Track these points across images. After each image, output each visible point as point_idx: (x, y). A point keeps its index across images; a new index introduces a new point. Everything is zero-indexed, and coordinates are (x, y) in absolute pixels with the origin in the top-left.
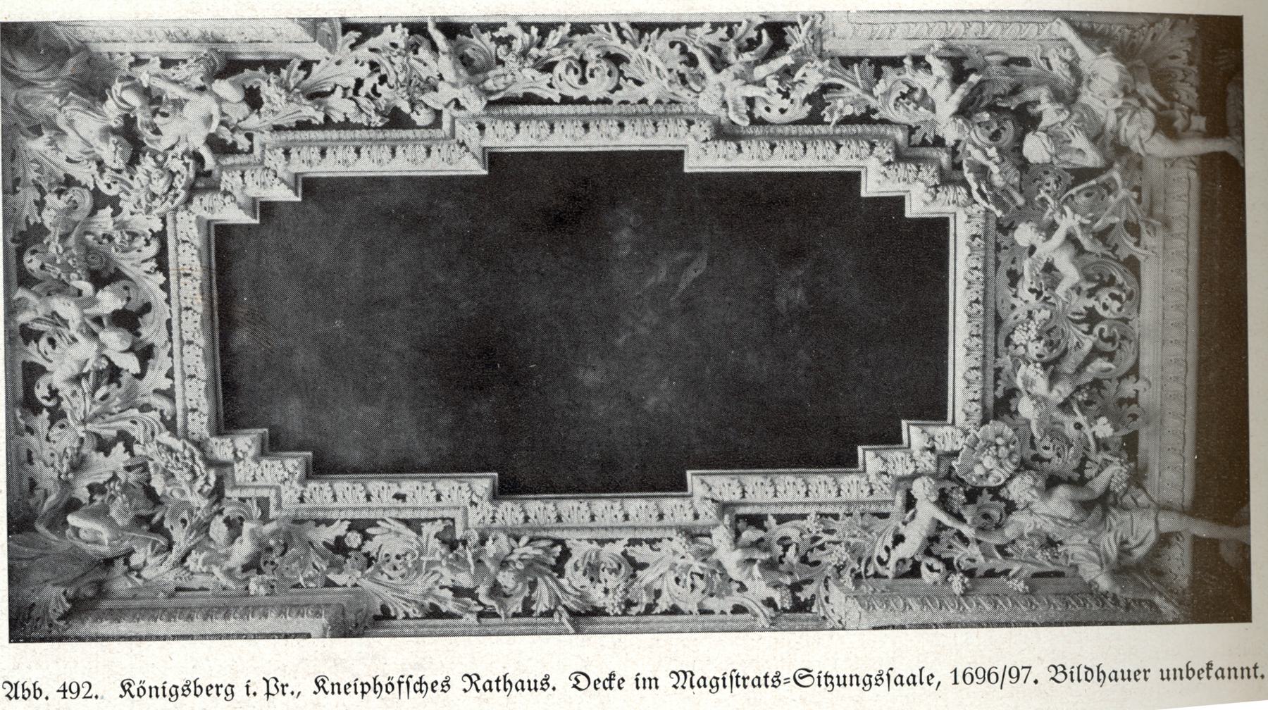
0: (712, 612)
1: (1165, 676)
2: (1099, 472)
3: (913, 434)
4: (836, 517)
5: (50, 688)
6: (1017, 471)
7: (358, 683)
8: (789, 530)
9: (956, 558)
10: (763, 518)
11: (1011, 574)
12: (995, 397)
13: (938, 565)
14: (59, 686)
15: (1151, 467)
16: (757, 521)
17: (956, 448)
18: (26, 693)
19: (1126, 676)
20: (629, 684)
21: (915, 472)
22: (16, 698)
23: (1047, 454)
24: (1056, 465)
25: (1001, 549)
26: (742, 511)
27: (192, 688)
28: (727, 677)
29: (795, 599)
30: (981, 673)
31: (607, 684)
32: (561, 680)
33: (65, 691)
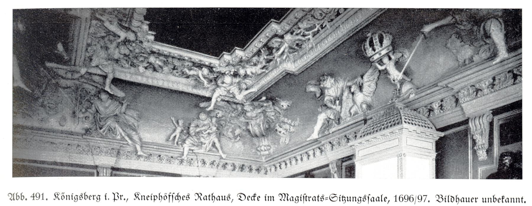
1: (484, 201)
5: (28, 195)
14: (31, 194)
18: (18, 198)
19: (223, 198)
20: (262, 199)
22: (14, 199)
27: (84, 196)
30: (406, 198)
31: (253, 198)
32: (234, 196)
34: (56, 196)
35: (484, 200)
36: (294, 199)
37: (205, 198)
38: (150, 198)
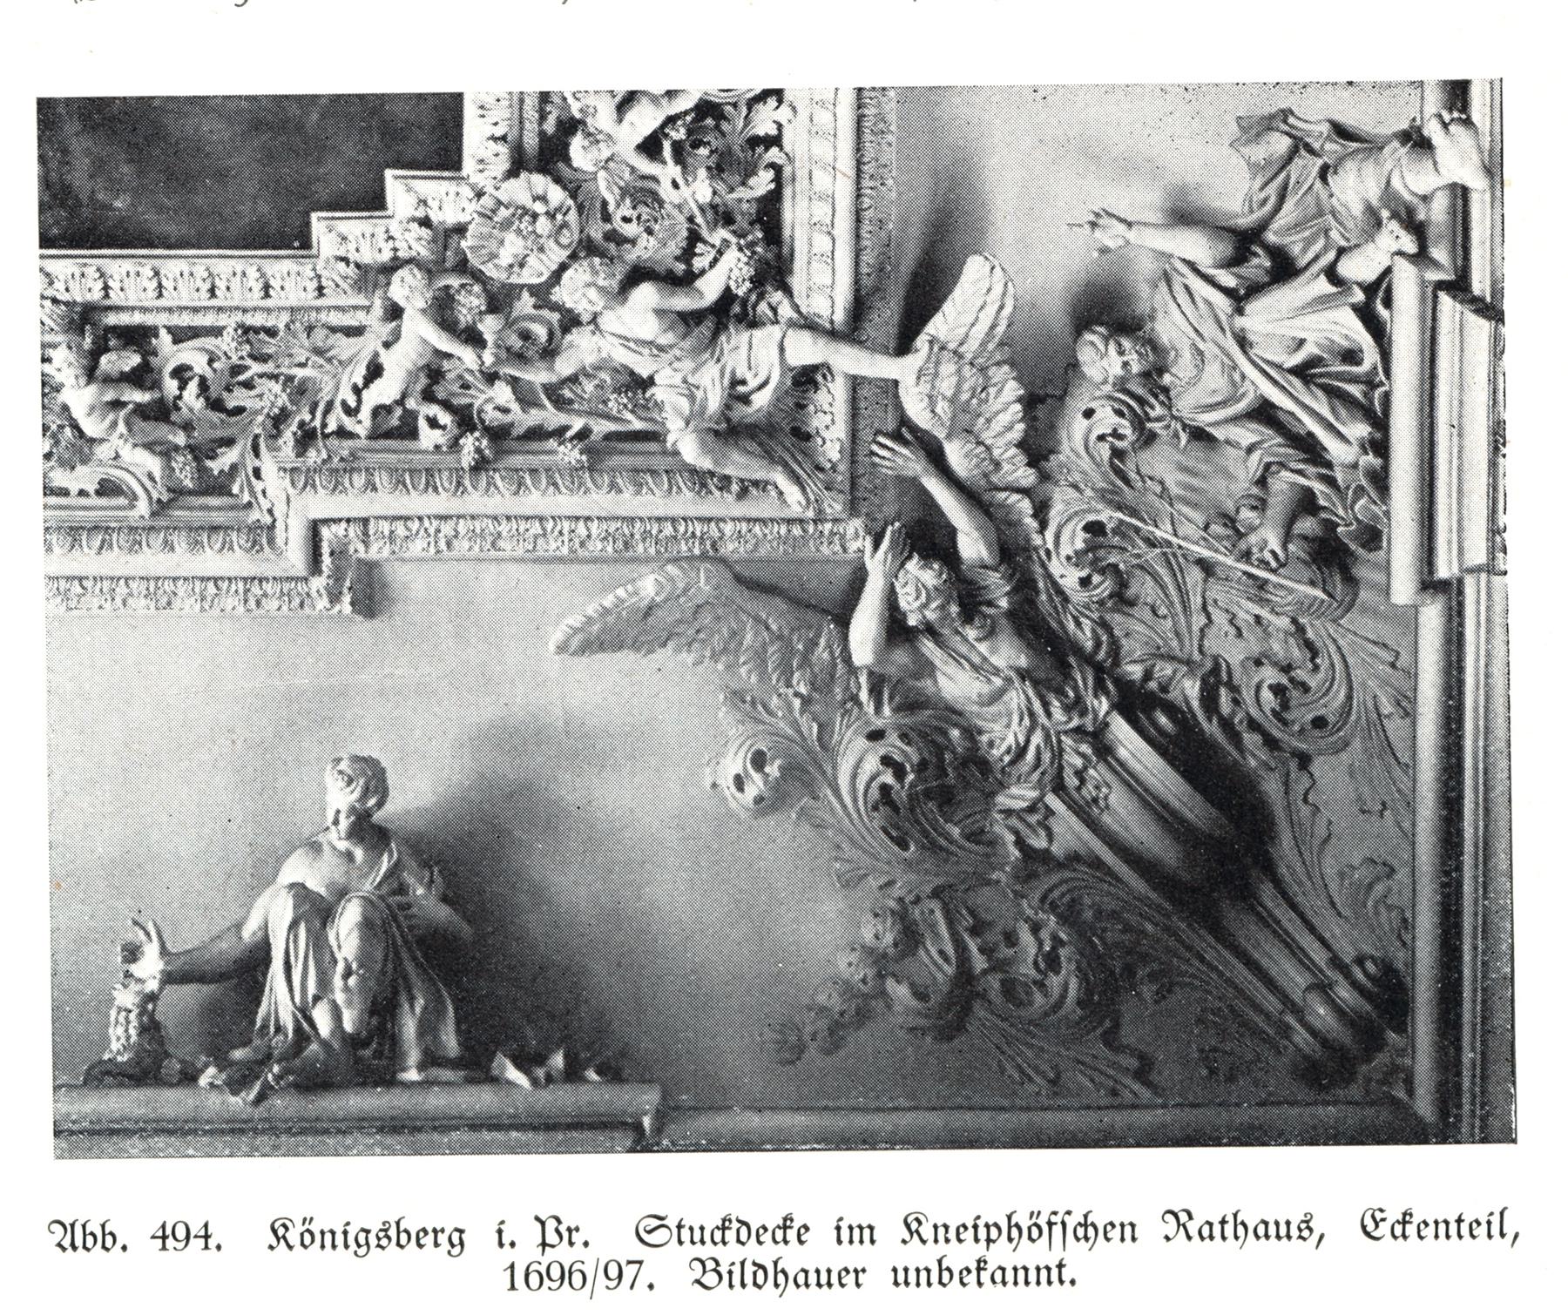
0: (65, 493)
2: (716, 260)
3: (400, 191)
4: (271, 332)
5: (135, 1229)
6: (574, 257)
7: (981, 1223)
8: (192, 355)
9: (477, 404)
10: (151, 331)
11: (569, 434)
12: (542, 134)
13: (445, 418)
14: (154, 1227)
15: (797, 255)
16: (138, 337)
17: (464, 218)
18: (90, 1240)
21: (395, 258)
22: (861, 1228)
23: (630, 230)
24: (645, 249)
25: (552, 391)
26: (112, 319)
27: (394, 1234)
29: (202, 471)
31: (779, 1235)
33: (164, 1238)
34: (279, 1231)
35: (901, 1279)
37: (1206, 1232)
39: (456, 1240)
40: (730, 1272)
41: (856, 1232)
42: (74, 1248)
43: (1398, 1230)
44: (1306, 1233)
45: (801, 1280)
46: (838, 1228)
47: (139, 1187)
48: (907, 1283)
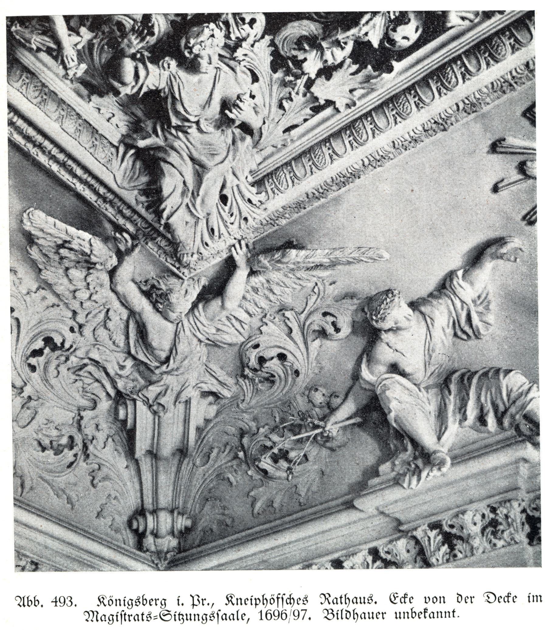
5: (46, 599)
7: (253, 598)
18: (30, 603)
28: (119, 615)
31: (506, 599)
33: (56, 602)
35: (398, 616)
36: (107, 619)
37: (335, 601)
38: (249, 602)
39: (163, 603)
40: (337, 614)
41: (535, 598)
42: (24, 606)
43: (403, 600)
44: (370, 601)
45: (363, 616)
46: (529, 597)
47: (44, 584)
48: (191, 620)
